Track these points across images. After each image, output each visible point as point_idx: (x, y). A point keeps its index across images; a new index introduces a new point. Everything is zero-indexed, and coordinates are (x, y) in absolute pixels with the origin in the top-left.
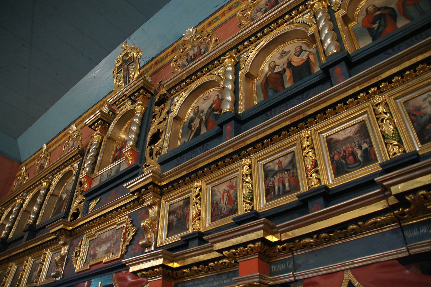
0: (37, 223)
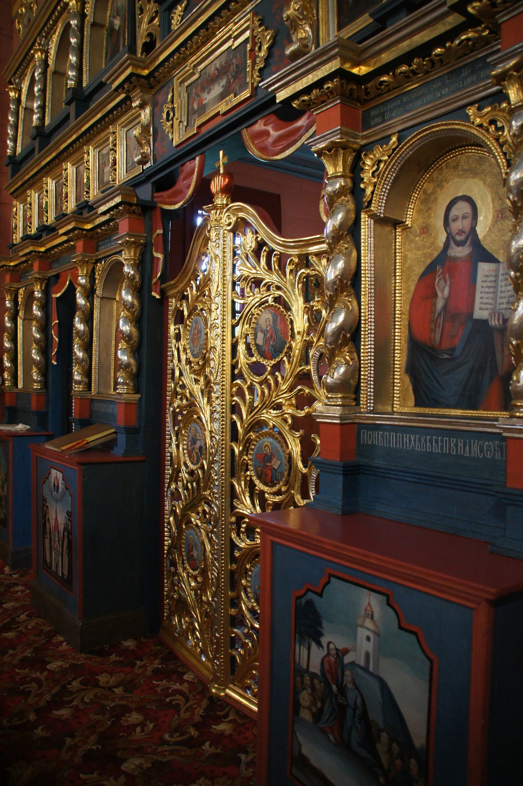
0: (84, 85)
